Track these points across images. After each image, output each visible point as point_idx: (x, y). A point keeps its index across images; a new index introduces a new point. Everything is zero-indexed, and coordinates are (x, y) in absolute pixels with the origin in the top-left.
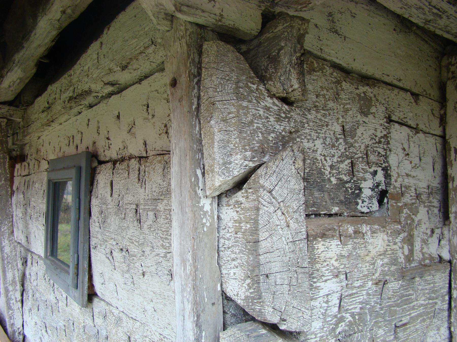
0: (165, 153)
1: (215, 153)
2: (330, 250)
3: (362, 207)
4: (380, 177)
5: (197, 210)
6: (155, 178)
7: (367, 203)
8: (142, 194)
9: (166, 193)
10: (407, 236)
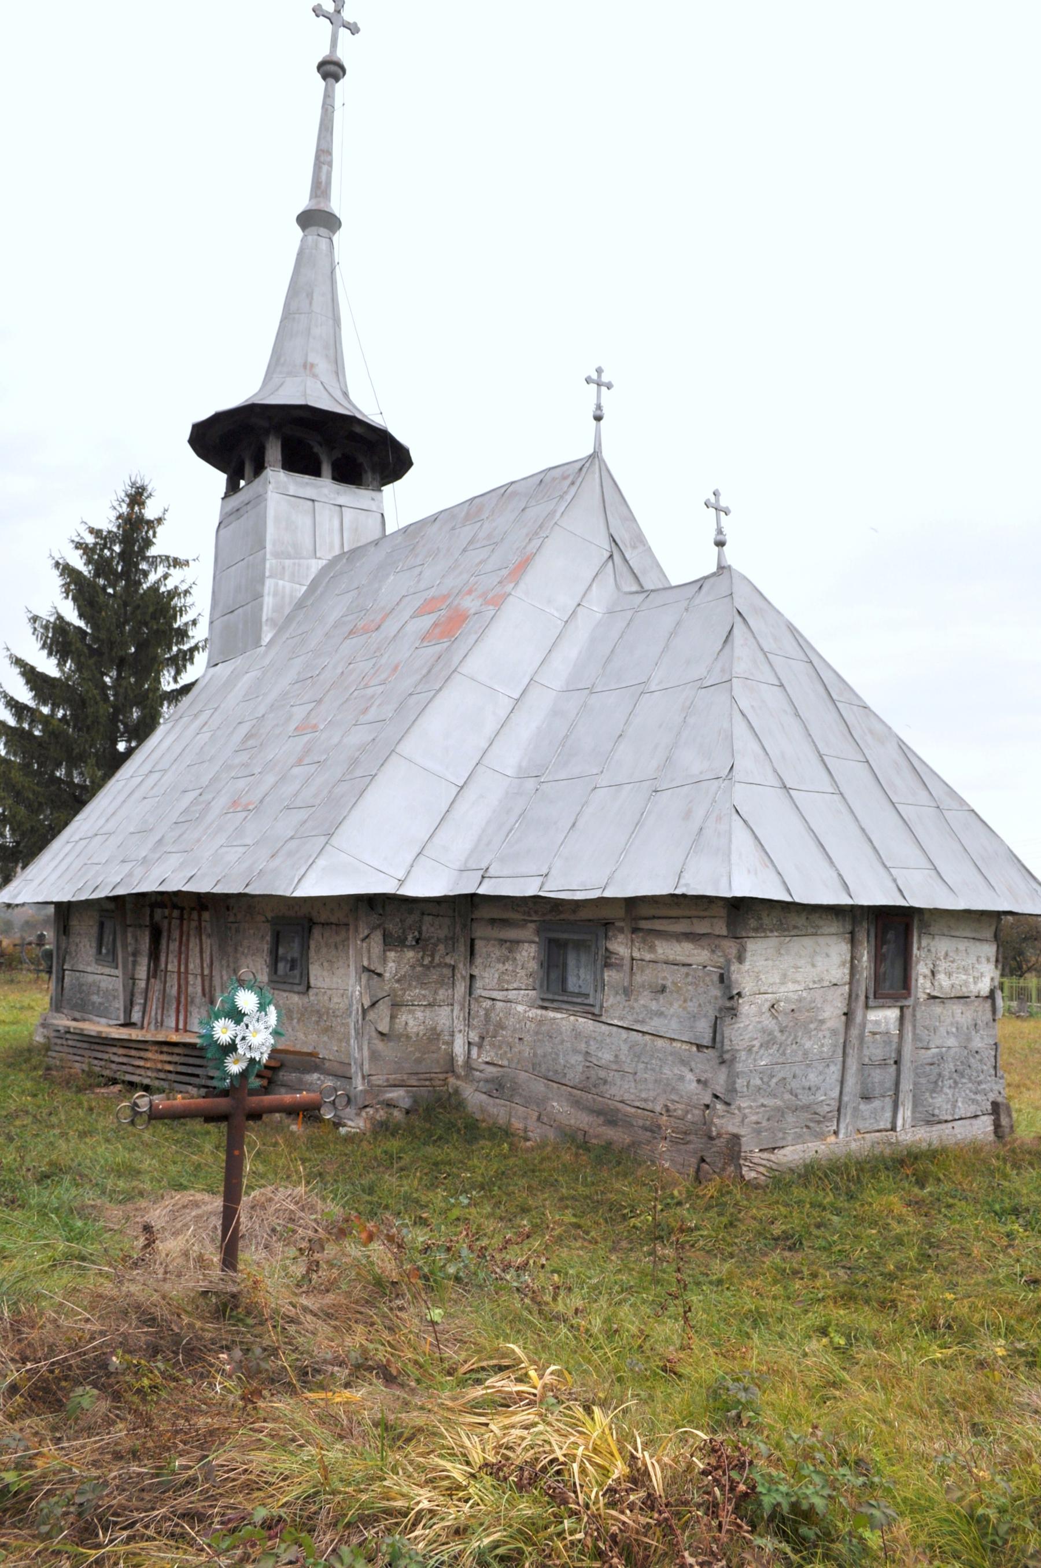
0: (347, 925)
1: (361, 930)
2: (391, 955)
3: (408, 943)
4: (416, 933)
5: (356, 944)
6: (343, 934)
7: (410, 940)
8: (338, 939)
9: (348, 939)
10: (79, 934)
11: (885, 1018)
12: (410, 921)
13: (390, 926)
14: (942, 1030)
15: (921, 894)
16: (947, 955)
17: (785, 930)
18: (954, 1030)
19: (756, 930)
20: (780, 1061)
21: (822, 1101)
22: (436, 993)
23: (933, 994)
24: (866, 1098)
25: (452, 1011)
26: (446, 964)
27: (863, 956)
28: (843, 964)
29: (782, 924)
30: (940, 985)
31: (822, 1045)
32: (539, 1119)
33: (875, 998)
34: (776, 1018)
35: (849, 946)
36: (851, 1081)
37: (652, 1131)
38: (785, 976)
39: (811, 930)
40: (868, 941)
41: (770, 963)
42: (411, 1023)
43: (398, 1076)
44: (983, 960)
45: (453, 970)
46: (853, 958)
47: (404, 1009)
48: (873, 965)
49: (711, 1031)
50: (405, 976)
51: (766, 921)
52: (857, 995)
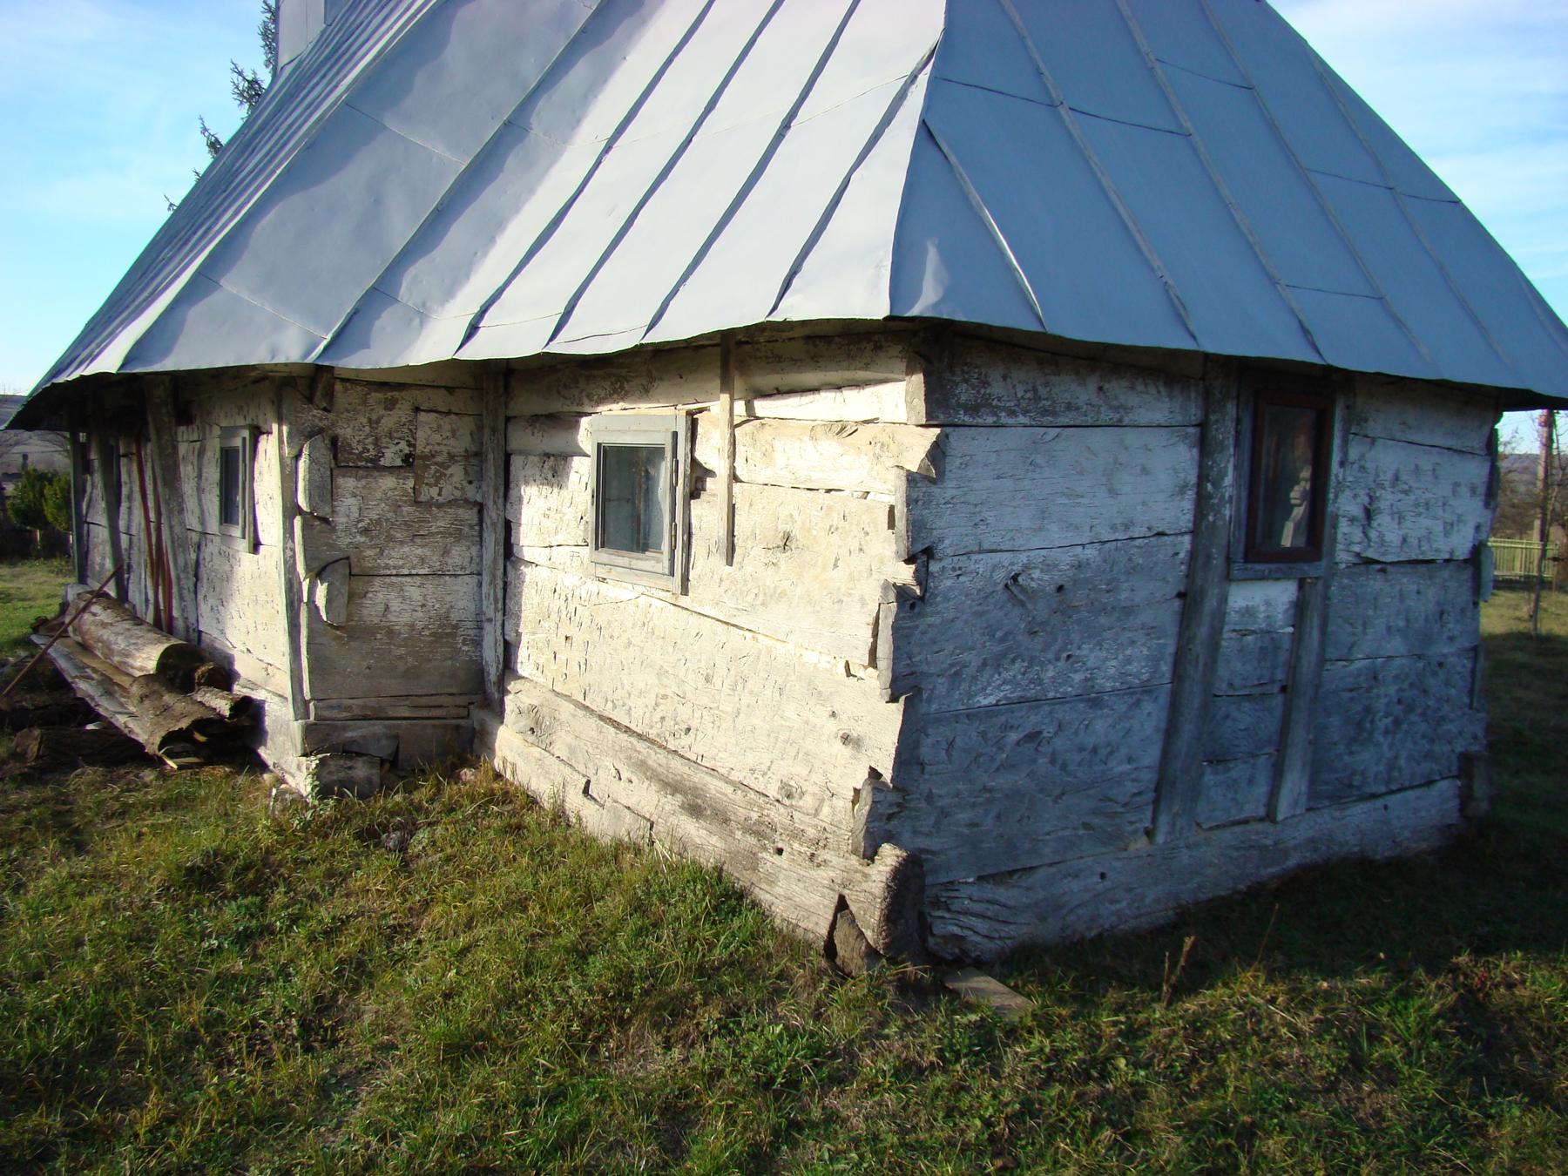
4: (403, 445)
11: (1267, 603)
12: (389, 421)
13: (345, 431)
14: (1380, 624)
15: (1352, 348)
16: (1397, 478)
17: (1045, 412)
18: (1401, 624)
19: (973, 409)
20: (1031, 693)
21: (1122, 774)
22: (446, 553)
23: (1370, 554)
24: (1218, 759)
25: (480, 584)
26: (466, 501)
27: (1222, 474)
28: (1182, 490)
29: (1037, 398)
30: (1381, 536)
31: (1128, 661)
32: (586, 791)
33: (1246, 560)
34: (1023, 604)
35: (1195, 451)
36: (1187, 730)
37: (757, 834)
38: (1043, 513)
39: (1107, 415)
40: (1237, 445)
41: (1008, 483)
42: (395, 605)
43: (372, 702)
44: (1464, 491)
45: (480, 512)
46: (1202, 478)
47: (377, 581)
48: (1244, 494)
49: (869, 631)
50: (379, 521)
51: (997, 388)
52: (1209, 557)
